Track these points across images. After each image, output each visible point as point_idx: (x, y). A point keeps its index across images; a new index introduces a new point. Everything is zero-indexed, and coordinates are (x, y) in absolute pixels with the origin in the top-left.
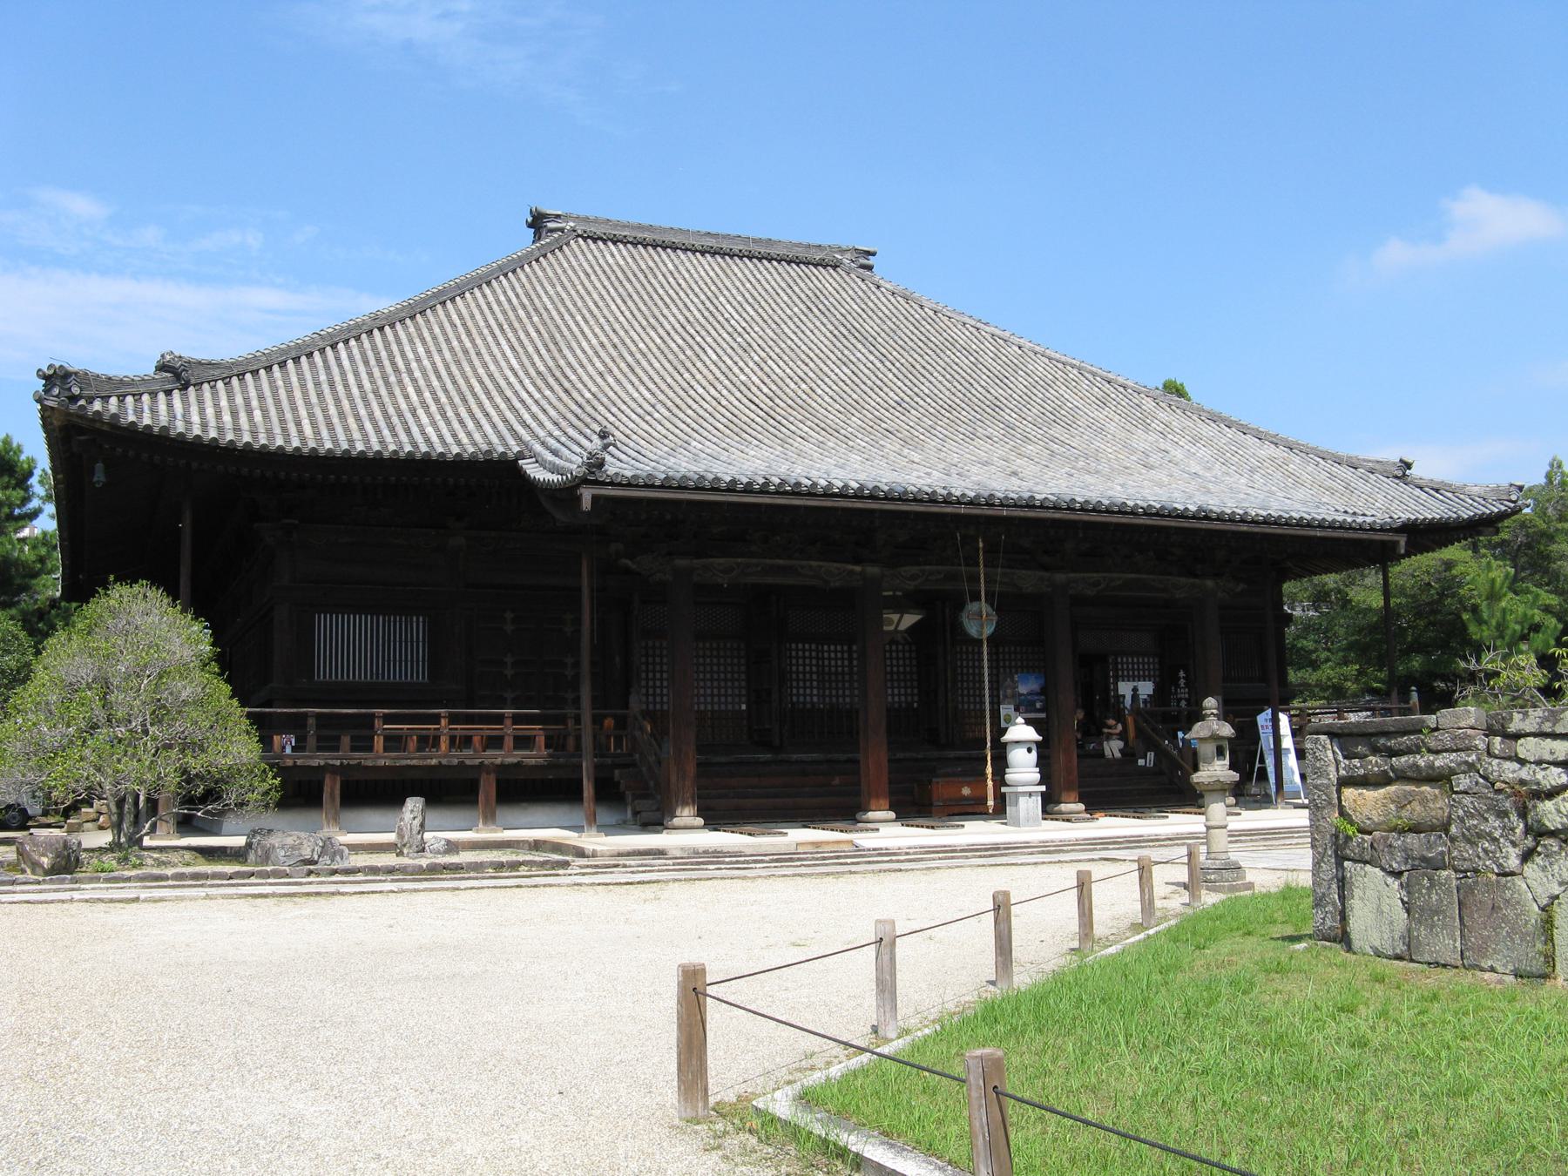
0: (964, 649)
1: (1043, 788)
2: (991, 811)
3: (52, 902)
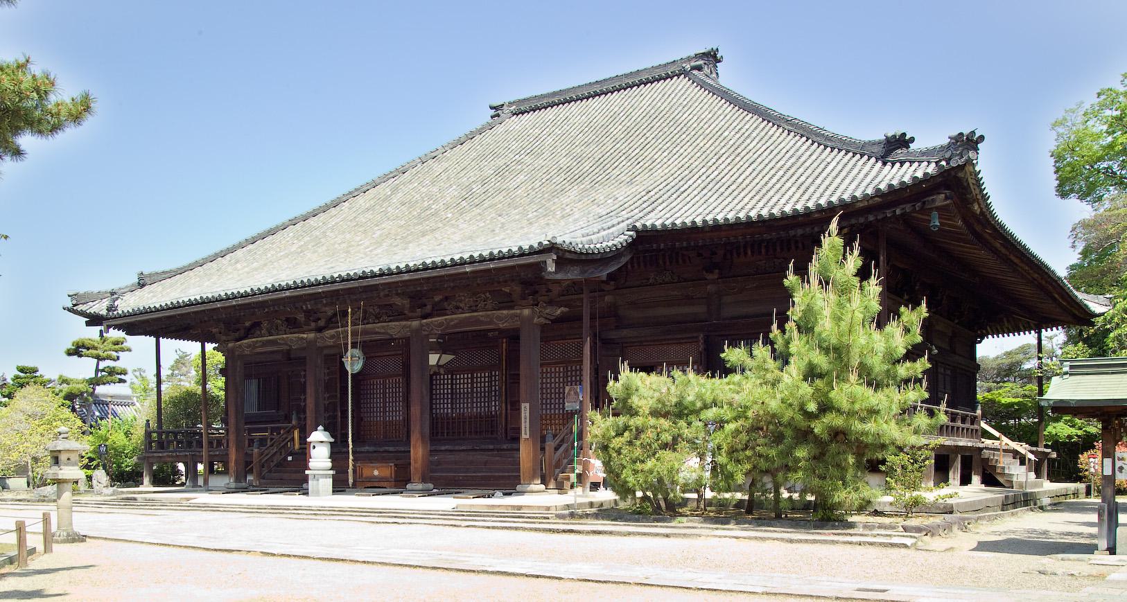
1: (307, 472)
2: (350, 486)
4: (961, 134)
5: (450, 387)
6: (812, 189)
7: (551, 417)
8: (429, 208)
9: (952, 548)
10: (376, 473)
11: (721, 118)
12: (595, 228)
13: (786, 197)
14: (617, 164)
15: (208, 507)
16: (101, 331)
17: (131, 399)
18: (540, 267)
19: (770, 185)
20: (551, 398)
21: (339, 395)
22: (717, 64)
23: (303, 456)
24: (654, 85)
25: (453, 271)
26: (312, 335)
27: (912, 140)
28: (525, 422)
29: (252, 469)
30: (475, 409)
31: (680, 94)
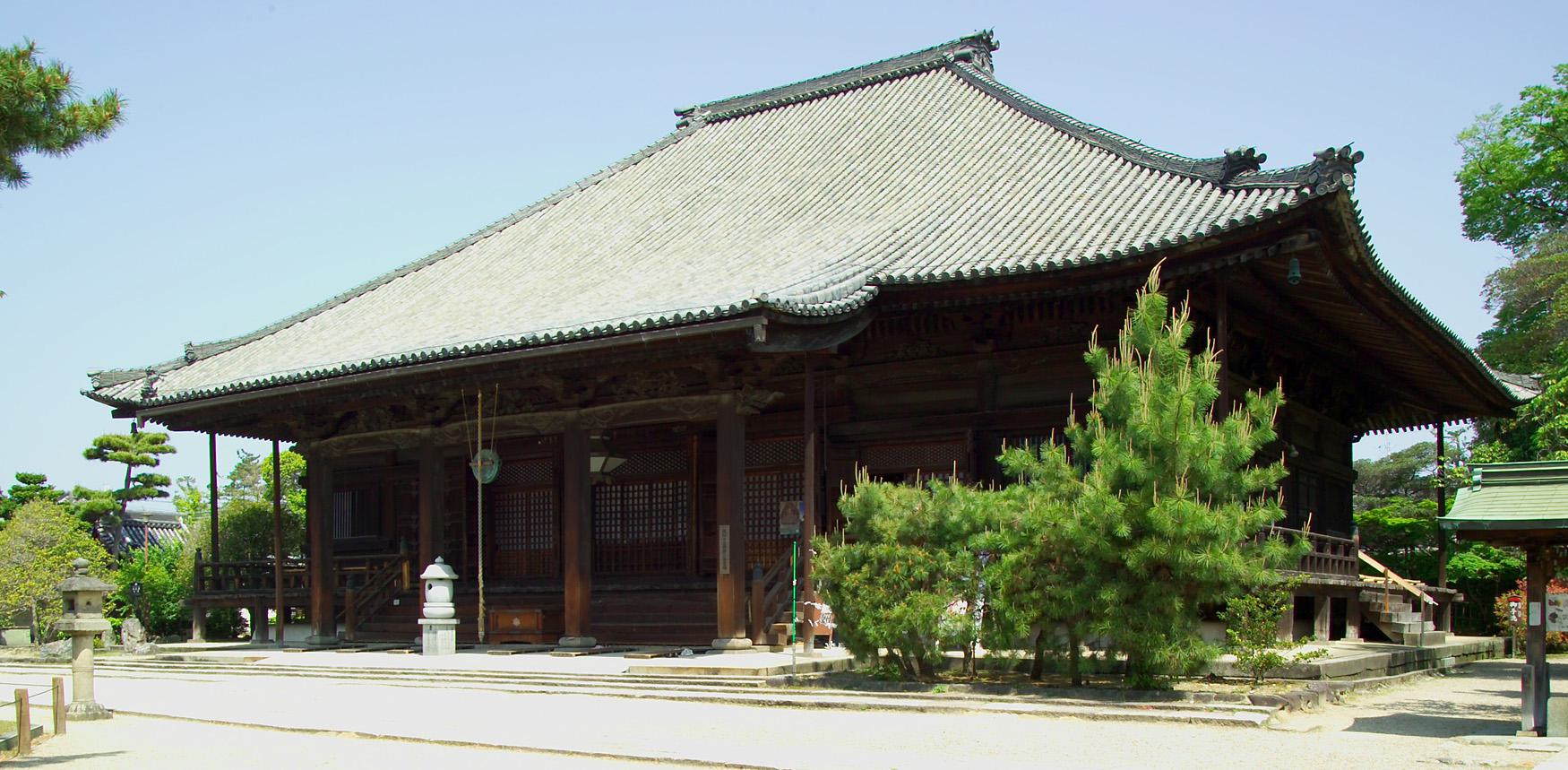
0: (757, 480)
2: (481, 640)
3: (460, 681)
4: (1331, 150)
6: (1123, 227)
7: (760, 545)
9: (1318, 727)
10: (517, 622)
13: (1088, 238)
15: (283, 670)
16: (134, 425)
17: (175, 520)
18: (744, 335)
19: (1065, 221)
24: (903, 81)
26: (426, 431)
27: (1263, 158)
28: (725, 551)
30: (654, 534)
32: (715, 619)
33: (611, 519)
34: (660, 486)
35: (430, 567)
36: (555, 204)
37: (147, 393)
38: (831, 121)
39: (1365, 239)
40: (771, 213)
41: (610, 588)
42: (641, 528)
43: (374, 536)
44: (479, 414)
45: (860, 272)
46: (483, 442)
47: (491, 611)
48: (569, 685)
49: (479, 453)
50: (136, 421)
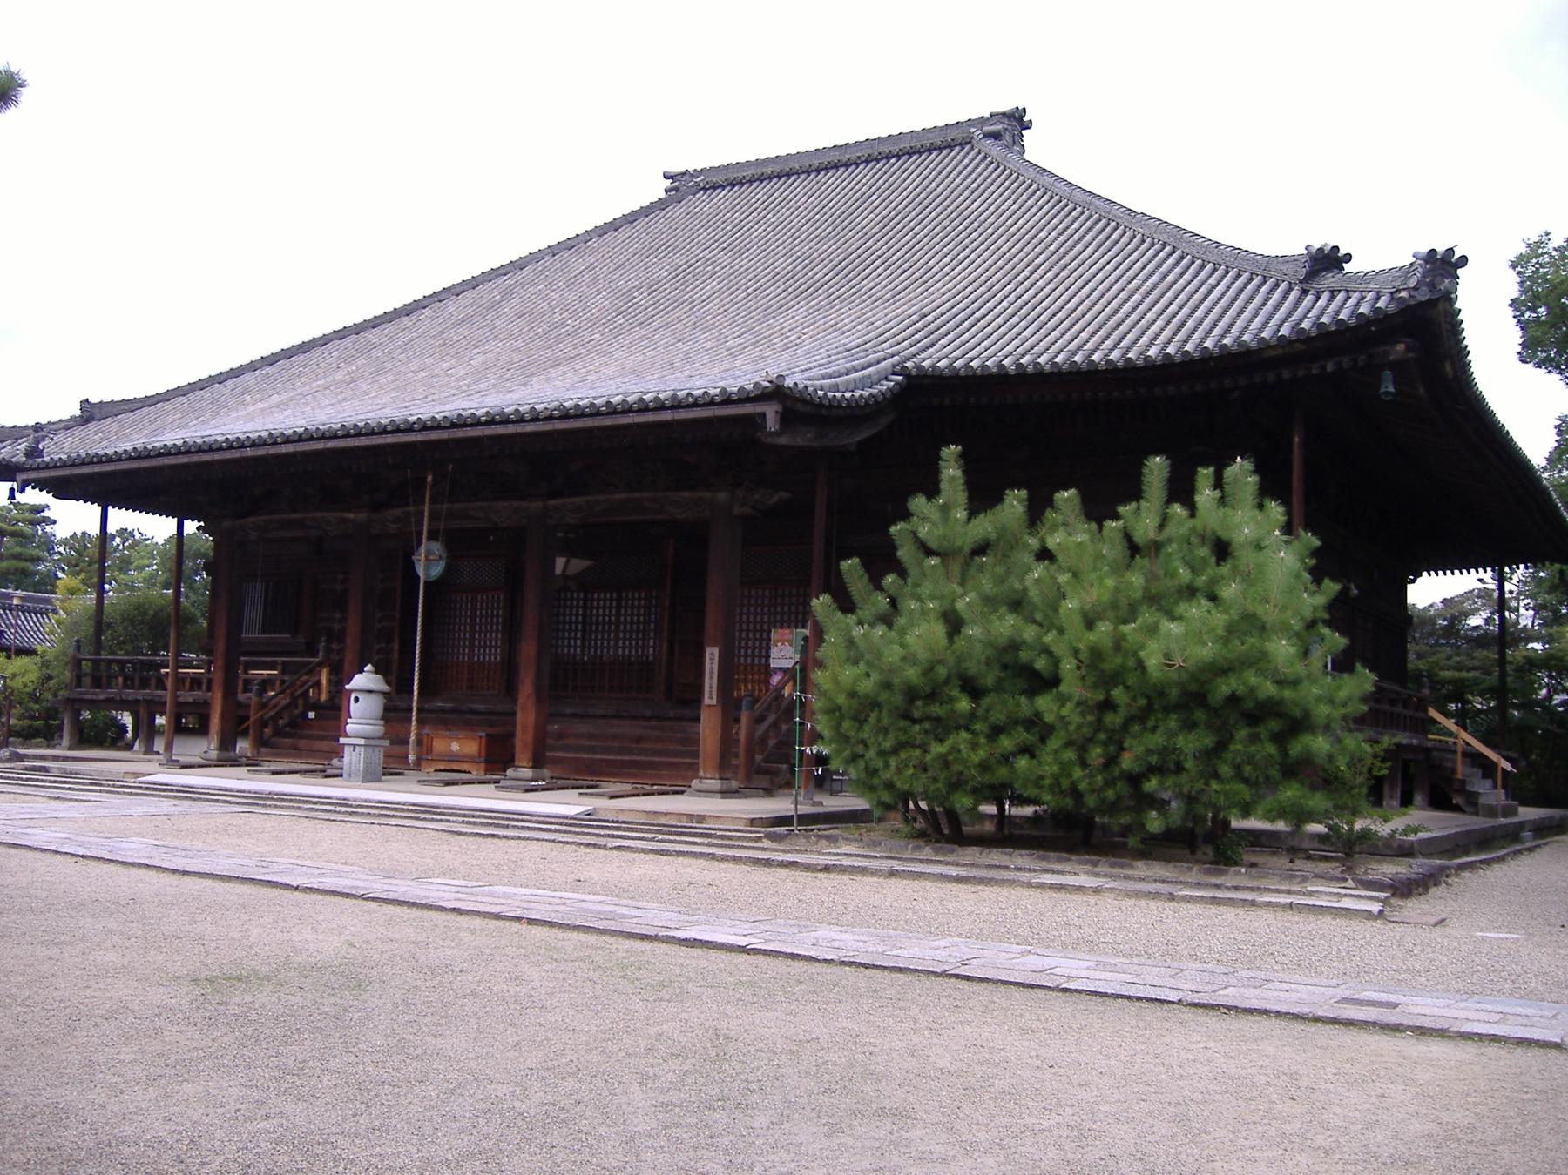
1: (342, 740)
4: (1433, 251)
5: (581, 612)
6: (1190, 324)
7: (746, 670)
8: (563, 324)
9: (1443, 920)
10: (455, 747)
11: (1034, 210)
12: (843, 365)
13: (1150, 333)
14: (867, 271)
15: (172, 790)
16: (12, 490)
17: (52, 604)
18: (756, 421)
19: (1120, 314)
20: (748, 639)
21: (398, 616)
22: (1023, 132)
23: (335, 710)
24: (923, 156)
25: (608, 421)
26: (362, 516)
27: (1348, 258)
28: (711, 678)
29: (248, 728)
30: (620, 651)
31: (965, 173)
32: (696, 754)
33: (632, 623)
34: (630, 595)
35: (358, 677)
36: (522, 269)
37: (33, 452)
38: (842, 194)
39: (1464, 352)
40: (774, 290)
41: (569, 711)
42: (634, 642)
43: (288, 636)
44: (427, 500)
45: (885, 359)
46: (429, 532)
47: (426, 731)
48: (523, 828)
49: (423, 546)
50: (15, 486)
